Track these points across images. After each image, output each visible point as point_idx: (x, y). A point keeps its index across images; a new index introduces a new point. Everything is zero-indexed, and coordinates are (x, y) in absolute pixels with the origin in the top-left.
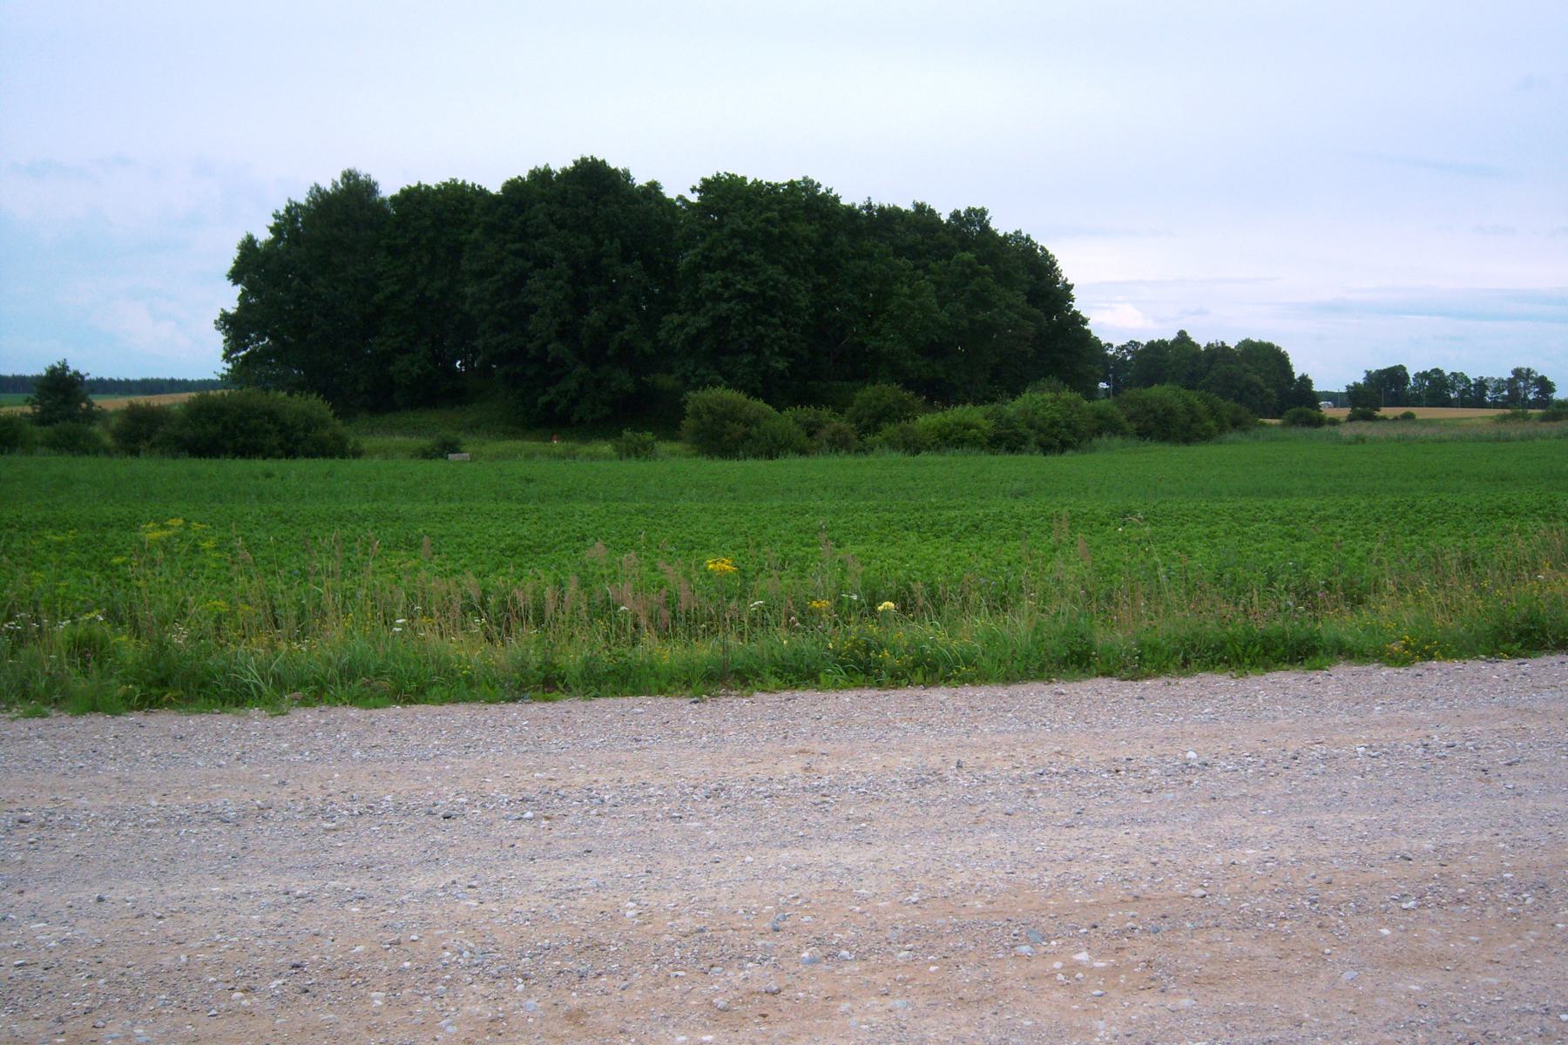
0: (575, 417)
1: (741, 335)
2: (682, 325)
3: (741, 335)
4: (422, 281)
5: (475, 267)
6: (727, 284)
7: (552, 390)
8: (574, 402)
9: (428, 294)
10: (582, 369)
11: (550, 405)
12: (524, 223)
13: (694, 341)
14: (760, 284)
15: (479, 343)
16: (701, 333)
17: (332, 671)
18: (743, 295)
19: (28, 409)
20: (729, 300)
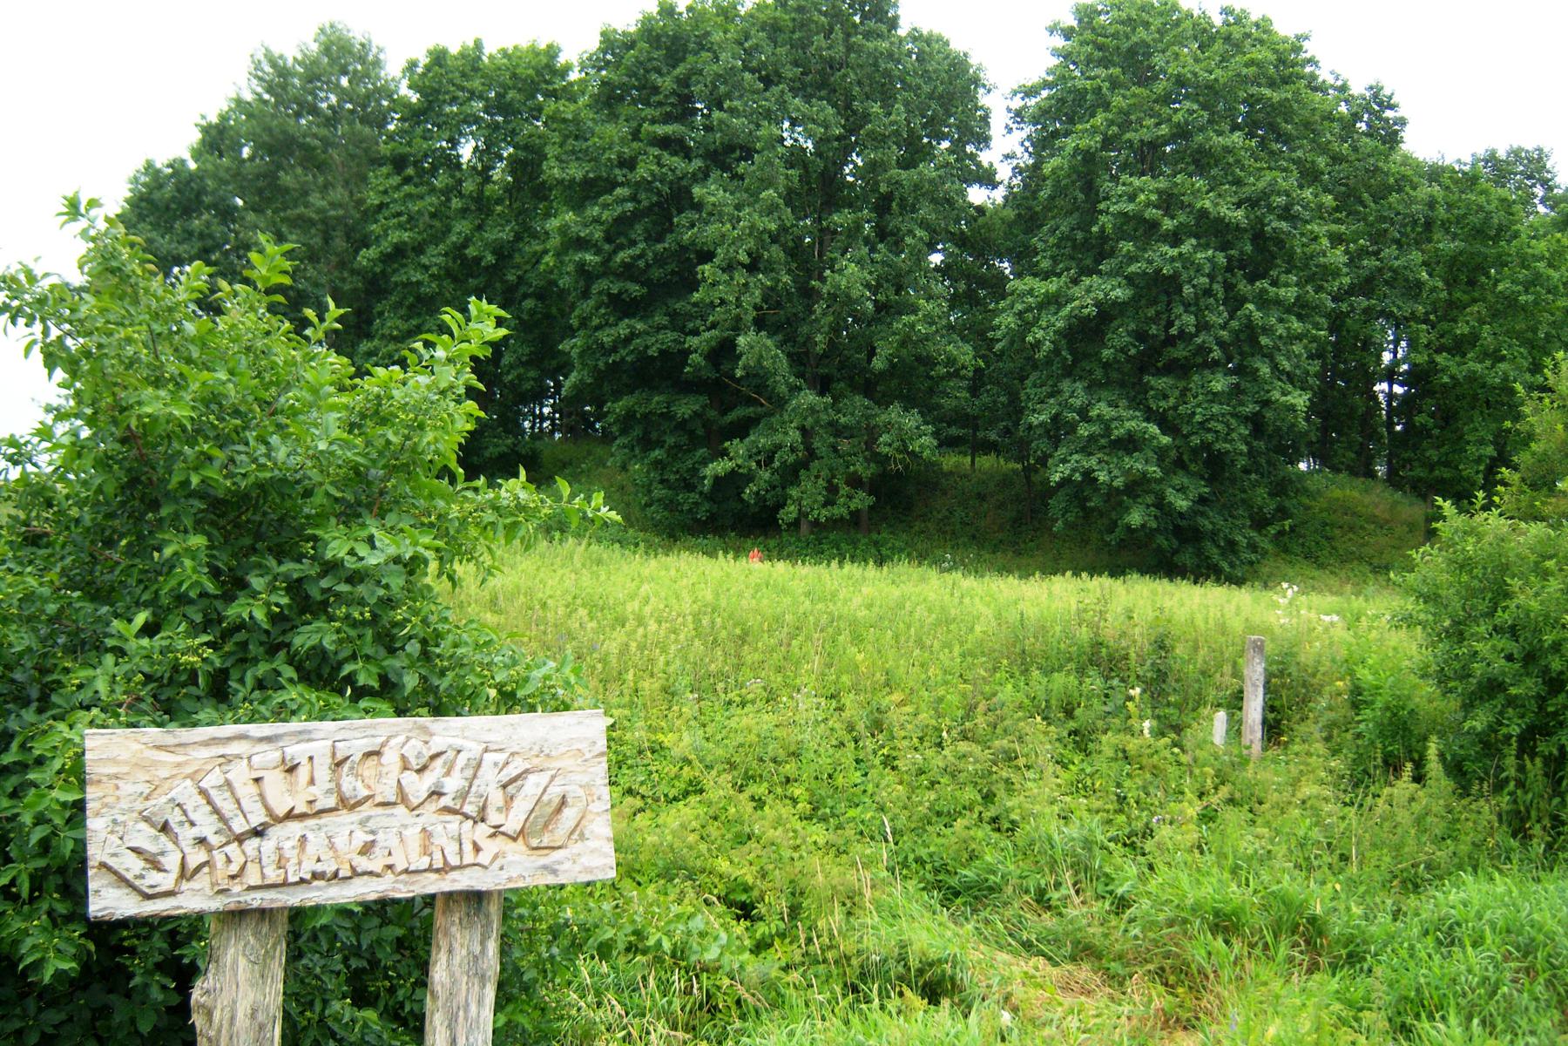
0: (789, 512)
1: (1203, 326)
2: (1054, 301)
3: (1203, 326)
4: (462, 227)
5: (576, 171)
6: (1168, 202)
7: (738, 448)
8: (791, 474)
9: (471, 252)
10: (809, 398)
11: (732, 482)
12: (684, 82)
13: (1086, 332)
14: (1252, 203)
15: (571, 346)
16: (1108, 312)
17: (992, 485)
18: (1212, 230)
19: (74, 965)
20: (1175, 239)
